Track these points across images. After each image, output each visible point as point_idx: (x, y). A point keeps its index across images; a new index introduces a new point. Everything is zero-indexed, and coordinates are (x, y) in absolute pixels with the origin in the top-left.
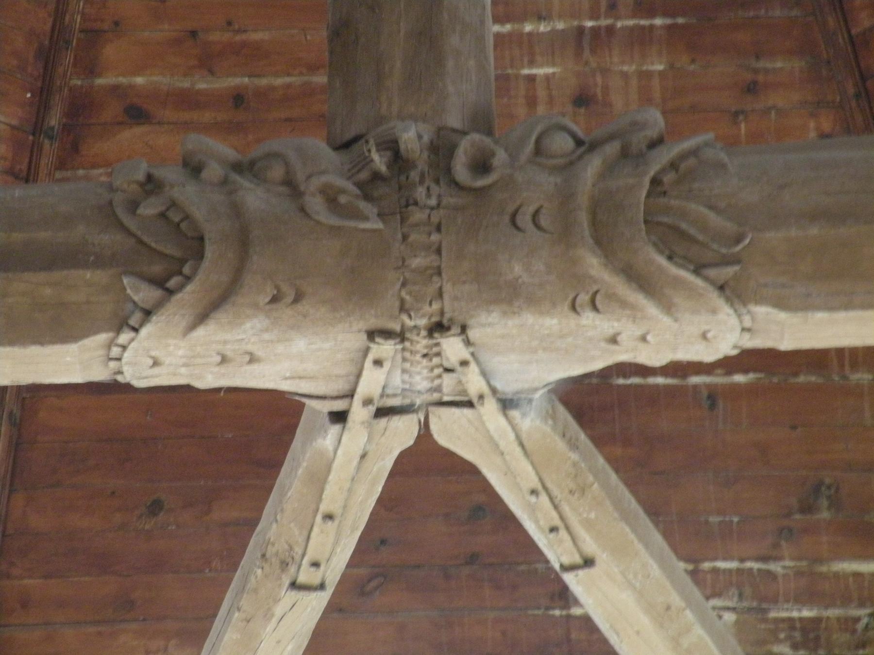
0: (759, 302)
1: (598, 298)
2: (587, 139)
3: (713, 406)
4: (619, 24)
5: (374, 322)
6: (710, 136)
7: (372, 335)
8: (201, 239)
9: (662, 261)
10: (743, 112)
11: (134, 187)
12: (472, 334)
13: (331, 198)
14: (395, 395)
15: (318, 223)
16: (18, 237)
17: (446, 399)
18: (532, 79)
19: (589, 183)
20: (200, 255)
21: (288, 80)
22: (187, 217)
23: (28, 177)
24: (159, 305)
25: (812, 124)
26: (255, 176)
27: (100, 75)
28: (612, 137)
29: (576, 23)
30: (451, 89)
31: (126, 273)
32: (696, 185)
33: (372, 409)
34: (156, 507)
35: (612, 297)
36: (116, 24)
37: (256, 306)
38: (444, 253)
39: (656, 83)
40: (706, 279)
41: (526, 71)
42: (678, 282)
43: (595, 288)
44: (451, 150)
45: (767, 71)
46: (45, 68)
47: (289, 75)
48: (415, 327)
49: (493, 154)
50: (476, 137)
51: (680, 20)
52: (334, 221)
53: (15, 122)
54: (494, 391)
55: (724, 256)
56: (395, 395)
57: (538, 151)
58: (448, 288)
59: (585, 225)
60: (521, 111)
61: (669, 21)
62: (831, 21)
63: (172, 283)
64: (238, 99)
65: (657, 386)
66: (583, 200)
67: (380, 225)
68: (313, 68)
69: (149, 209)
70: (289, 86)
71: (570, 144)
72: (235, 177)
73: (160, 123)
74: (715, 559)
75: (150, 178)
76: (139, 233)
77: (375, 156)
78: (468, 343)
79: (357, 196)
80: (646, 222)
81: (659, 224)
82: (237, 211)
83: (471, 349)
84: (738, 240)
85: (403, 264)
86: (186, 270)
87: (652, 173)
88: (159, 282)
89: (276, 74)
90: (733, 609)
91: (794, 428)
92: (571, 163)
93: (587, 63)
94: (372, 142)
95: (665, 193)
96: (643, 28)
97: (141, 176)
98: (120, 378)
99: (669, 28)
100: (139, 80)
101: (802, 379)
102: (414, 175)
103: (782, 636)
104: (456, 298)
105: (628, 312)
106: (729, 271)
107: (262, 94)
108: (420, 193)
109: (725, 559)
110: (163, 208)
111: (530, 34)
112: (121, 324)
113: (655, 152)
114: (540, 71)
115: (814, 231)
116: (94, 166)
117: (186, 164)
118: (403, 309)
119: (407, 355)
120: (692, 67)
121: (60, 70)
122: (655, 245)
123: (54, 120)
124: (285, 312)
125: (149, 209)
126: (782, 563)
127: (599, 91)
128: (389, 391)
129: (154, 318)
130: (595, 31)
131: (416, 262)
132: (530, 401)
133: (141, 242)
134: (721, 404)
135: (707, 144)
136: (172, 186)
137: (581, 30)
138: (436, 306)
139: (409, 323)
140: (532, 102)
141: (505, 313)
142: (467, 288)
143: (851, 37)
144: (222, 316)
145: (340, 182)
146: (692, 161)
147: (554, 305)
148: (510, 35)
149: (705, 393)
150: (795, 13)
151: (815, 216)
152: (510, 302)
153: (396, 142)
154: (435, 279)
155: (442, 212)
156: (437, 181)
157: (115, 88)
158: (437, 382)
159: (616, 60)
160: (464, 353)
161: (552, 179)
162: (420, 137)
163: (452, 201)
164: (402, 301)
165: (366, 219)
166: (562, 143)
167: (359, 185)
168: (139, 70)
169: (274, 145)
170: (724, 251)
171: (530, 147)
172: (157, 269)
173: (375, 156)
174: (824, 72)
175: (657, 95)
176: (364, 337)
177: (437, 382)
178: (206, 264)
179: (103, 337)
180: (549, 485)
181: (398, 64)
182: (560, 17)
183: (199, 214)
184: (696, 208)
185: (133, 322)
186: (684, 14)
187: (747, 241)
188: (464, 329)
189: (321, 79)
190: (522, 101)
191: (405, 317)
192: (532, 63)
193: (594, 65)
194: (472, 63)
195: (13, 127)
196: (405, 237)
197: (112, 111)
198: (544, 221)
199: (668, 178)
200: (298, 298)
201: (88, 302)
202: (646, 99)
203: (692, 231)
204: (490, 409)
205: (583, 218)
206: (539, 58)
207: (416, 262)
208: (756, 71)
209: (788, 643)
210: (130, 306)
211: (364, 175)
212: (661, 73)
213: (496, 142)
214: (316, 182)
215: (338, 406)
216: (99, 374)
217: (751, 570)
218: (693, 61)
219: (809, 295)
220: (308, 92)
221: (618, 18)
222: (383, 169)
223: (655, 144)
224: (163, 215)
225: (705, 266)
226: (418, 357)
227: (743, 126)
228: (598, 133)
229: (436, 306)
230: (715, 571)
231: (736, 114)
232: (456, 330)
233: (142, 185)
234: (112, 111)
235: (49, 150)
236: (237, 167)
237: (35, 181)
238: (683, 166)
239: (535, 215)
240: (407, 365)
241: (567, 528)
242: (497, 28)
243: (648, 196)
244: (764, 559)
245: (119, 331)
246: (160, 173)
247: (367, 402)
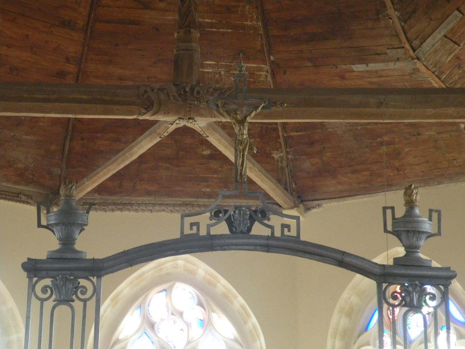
5: (179, 117)
13: (174, 97)
20: (153, 106)
22: (151, 98)
31: (142, 107)
34: (117, 45)
44: (194, 90)
49: (200, 91)
52: (174, 101)
57: (207, 91)
58: (192, 114)
63: (149, 109)
72: (159, 92)
74: (221, 62)
88: (146, 109)
90: (224, 71)
101: (241, 31)
103: (232, 76)
109: (223, 62)
118: (184, 116)
126: (233, 64)
129: (145, 115)
131: (187, 109)
144: (156, 115)
165: (179, 102)
171: (206, 90)
172: (146, 107)
180: (203, 130)
200: (168, 113)
207: (187, 109)
209: (233, 77)
214: (172, 94)
217: (228, 64)
230: (221, 64)
236: (159, 89)
241: (205, 134)
244: (230, 63)
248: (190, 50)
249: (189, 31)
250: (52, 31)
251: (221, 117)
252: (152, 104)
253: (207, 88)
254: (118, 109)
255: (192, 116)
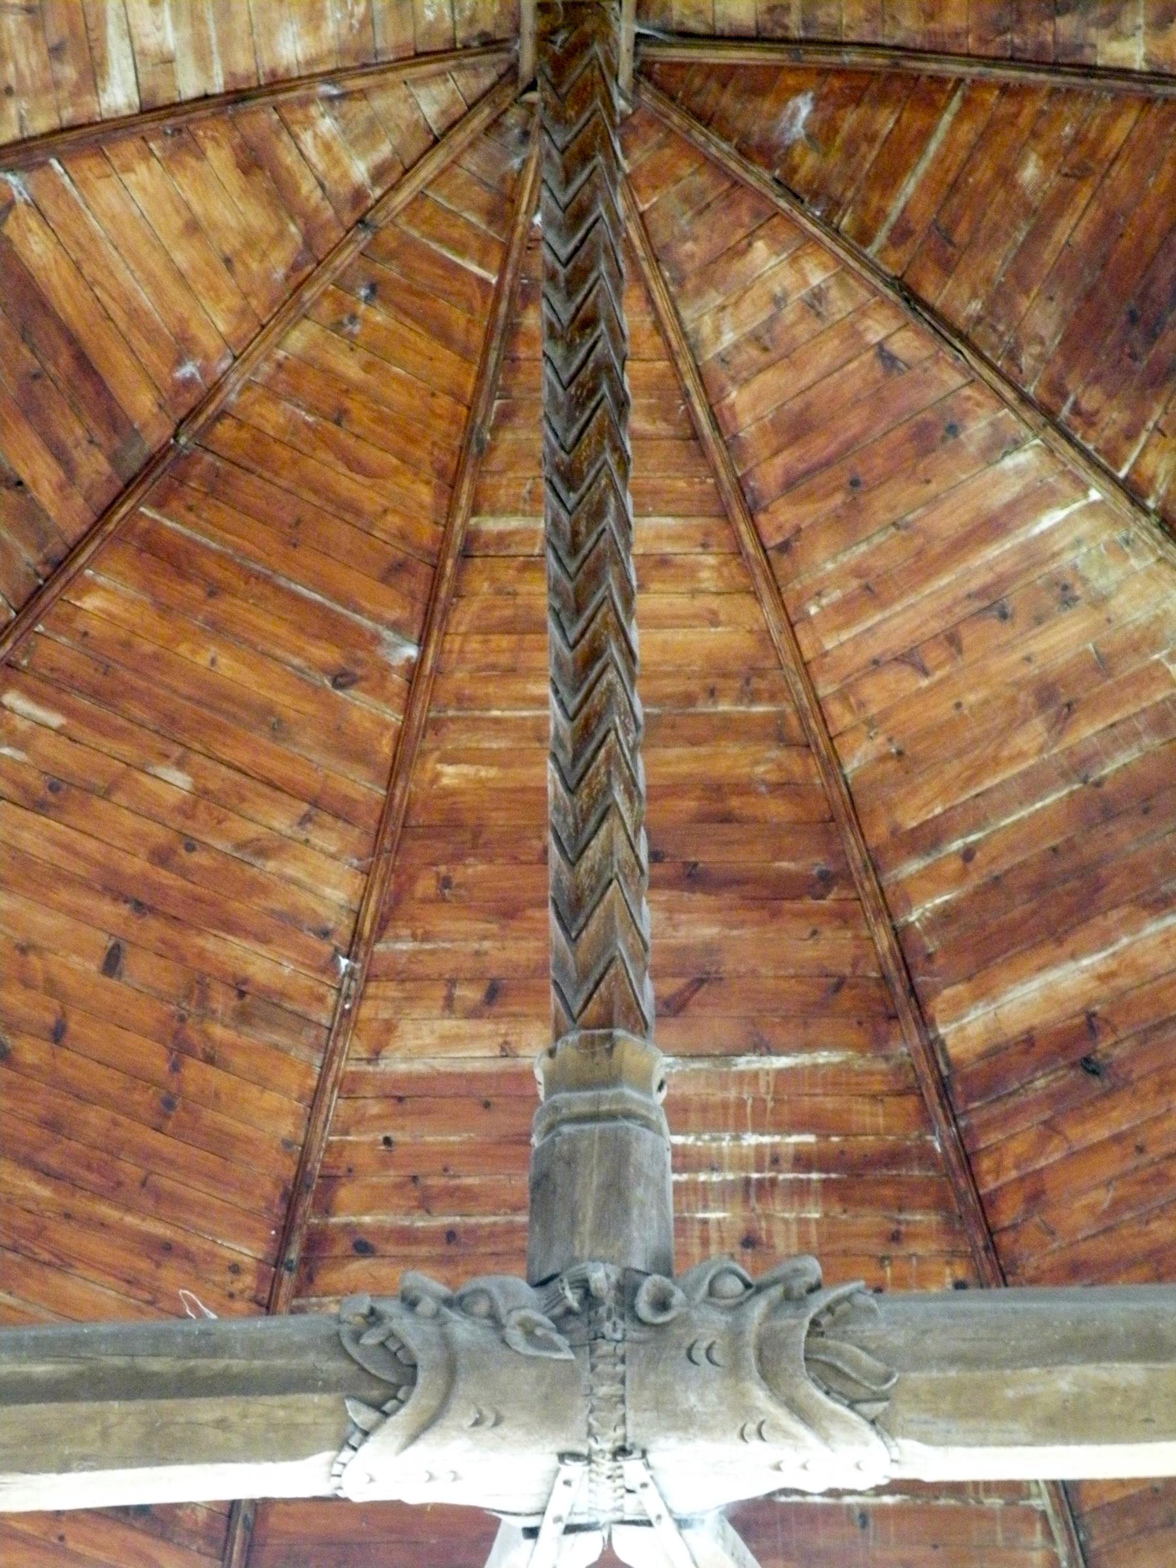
0: (906, 1435)
1: (764, 1427)
2: (754, 1283)
3: (864, 1524)
4: (781, 1177)
6: (861, 1284)
7: (562, 1457)
8: (415, 1366)
9: (820, 1395)
10: (888, 1258)
11: (359, 1319)
12: (650, 1457)
14: (582, 1514)
15: (517, 1352)
16: (257, 1363)
17: (628, 1518)
18: (705, 1222)
19: (756, 1321)
20: (413, 1382)
21: (492, 1219)
22: (403, 1347)
23: (268, 1307)
24: (377, 1426)
25: (948, 1271)
26: (463, 1310)
27: (334, 1215)
28: (775, 1282)
29: (743, 1175)
30: (635, 1234)
31: (348, 1397)
32: (849, 1328)
33: (561, 1526)
35: (776, 1427)
36: (350, 1170)
37: (460, 1428)
38: (628, 1383)
39: (813, 1229)
40: (859, 1413)
41: (700, 1215)
42: (834, 1414)
43: (761, 1418)
44: (635, 1289)
45: (908, 1223)
46: (289, 1208)
47: (495, 1214)
48: (601, 1450)
49: (672, 1294)
50: (656, 1277)
51: (833, 1176)
52: (531, 1351)
53: (260, 1256)
54: (670, 1512)
55: (874, 1393)
56: (582, 1514)
57: (712, 1292)
58: (630, 1415)
59: (753, 1361)
60: (696, 1250)
61: (823, 1176)
62: (962, 1183)
63: (388, 1407)
64: (451, 1236)
65: (815, 1505)
66: (751, 1337)
67: (572, 1357)
68: (516, 1209)
69: (371, 1339)
70: (495, 1224)
71: (740, 1286)
72: (446, 1310)
73: (383, 1256)
75: (373, 1312)
76: (361, 1361)
77: (569, 1294)
78: (648, 1466)
79: (551, 1329)
80: (806, 1359)
81: (817, 1361)
82: (446, 1342)
83: (650, 1472)
84: (887, 1379)
85: (590, 1393)
86: (401, 1395)
87: (811, 1315)
88: (377, 1406)
89: (484, 1214)
91: (935, 1547)
92: (741, 1304)
93: (753, 1210)
94: (566, 1280)
95: (822, 1334)
96: (801, 1181)
97: (365, 1310)
98: (341, 1494)
99: (824, 1181)
100: (367, 1219)
102: (602, 1311)
104: (638, 1425)
105: (790, 1441)
106: (879, 1407)
107: (471, 1231)
108: (607, 1327)
110: (382, 1338)
111: (704, 1183)
112: (343, 1443)
113: (814, 1297)
114: (713, 1215)
115: (952, 1373)
116: (325, 1295)
117: (404, 1299)
118: (590, 1433)
119: (593, 1476)
120: (844, 1217)
121: (301, 1211)
122: (814, 1380)
123: (294, 1254)
124: (486, 1434)
125: (371, 1339)
127: (763, 1235)
128: (576, 1510)
129: (371, 1438)
130: (760, 1182)
131: (603, 1390)
132: (703, 1521)
133: (363, 1369)
134: (871, 1522)
135: (859, 1291)
136: (391, 1318)
137: (748, 1181)
138: (620, 1431)
139: (596, 1447)
140: (705, 1242)
141: (681, 1439)
142: (648, 1414)
143: (979, 1197)
145: (538, 1317)
146: (846, 1306)
147: (724, 1433)
148: (687, 1183)
149: (857, 1512)
150: (931, 1174)
151: (954, 1359)
152: (685, 1429)
153: (586, 1281)
154: (620, 1406)
155: (626, 1345)
156: (622, 1317)
157: (347, 1225)
158: (620, 1502)
159: (778, 1208)
160: (645, 1476)
161: (723, 1318)
162: (608, 1276)
163: (635, 1335)
164: (590, 1426)
165: (559, 1350)
166: (732, 1286)
167: (554, 1319)
168: (367, 1210)
169: (481, 1282)
170: (874, 1388)
172: (375, 1394)
173: (569, 1294)
174: (958, 1226)
175: (814, 1239)
176: (556, 1458)
177: (620, 1502)
178: (418, 1390)
179: (328, 1455)
181: (590, 1213)
182: (731, 1169)
183: (413, 1343)
184: (848, 1347)
185: (353, 1442)
186: (835, 1171)
187: (894, 1380)
188: (644, 1453)
189: (522, 1218)
190: (697, 1241)
191: (591, 1441)
192: (705, 1208)
193: (759, 1211)
194: (654, 1212)
195: (260, 1261)
196: (593, 1367)
197: (342, 1246)
198: (716, 1356)
199: (825, 1320)
200: (498, 1422)
201: (315, 1424)
202: (805, 1247)
203: (847, 1369)
204: (667, 1526)
205: (751, 1353)
206: (711, 1204)
207: (603, 1390)
208: (899, 1222)
210: (351, 1427)
211: (558, 1311)
212: (816, 1220)
213: (675, 1283)
214: (516, 1316)
215: (531, 1522)
216: (324, 1489)
218: (845, 1211)
219: (949, 1432)
220: (511, 1230)
221: (780, 1171)
222: (575, 1305)
223: (814, 1289)
224: (382, 1344)
225: (858, 1401)
226: (603, 1479)
227: (888, 1270)
228: (764, 1277)
229: (620, 1431)
231: (883, 1259)
232: (637, 1454)
233: (365, 1317)
234: (342, 1246)
235: (289, 1279)
236: (448, 1302)
237: (274, 1313)
238: (839, 1309)
239: (709, 1350)
240: (593, 1486)
242: (675, 1177)
243: (809, 1334)
245: (340, 1449)
246: (381, 1306)
247: (558, 1519)
248: (612, 1116)
249: (609, 1037)
250: (61, 1538)
251: (799, 1429)
252: (409, 1373)
253: (713, 1272)
254: (222, 1424)
255: (633, 1434)
